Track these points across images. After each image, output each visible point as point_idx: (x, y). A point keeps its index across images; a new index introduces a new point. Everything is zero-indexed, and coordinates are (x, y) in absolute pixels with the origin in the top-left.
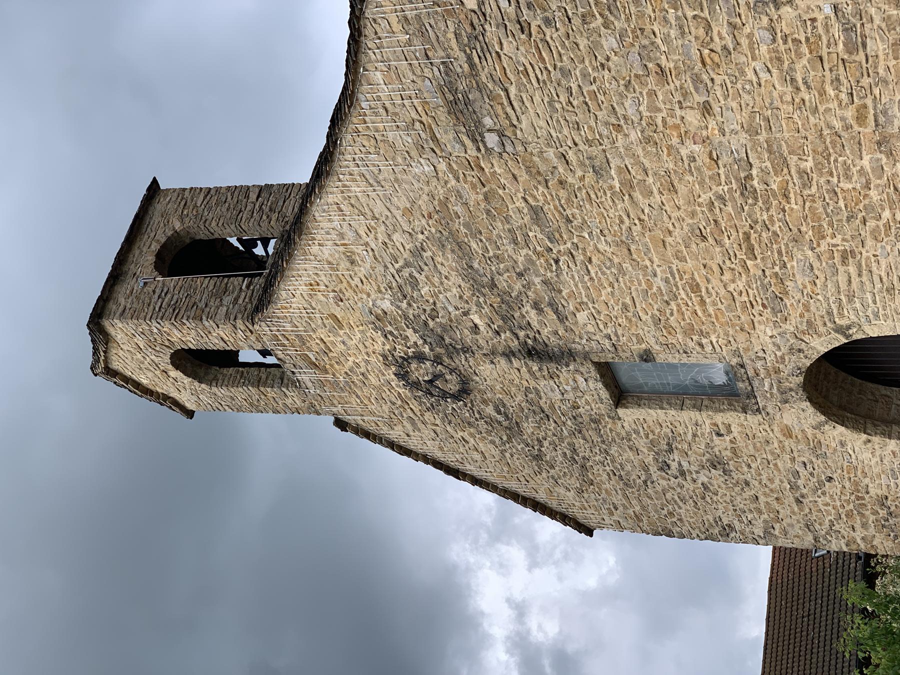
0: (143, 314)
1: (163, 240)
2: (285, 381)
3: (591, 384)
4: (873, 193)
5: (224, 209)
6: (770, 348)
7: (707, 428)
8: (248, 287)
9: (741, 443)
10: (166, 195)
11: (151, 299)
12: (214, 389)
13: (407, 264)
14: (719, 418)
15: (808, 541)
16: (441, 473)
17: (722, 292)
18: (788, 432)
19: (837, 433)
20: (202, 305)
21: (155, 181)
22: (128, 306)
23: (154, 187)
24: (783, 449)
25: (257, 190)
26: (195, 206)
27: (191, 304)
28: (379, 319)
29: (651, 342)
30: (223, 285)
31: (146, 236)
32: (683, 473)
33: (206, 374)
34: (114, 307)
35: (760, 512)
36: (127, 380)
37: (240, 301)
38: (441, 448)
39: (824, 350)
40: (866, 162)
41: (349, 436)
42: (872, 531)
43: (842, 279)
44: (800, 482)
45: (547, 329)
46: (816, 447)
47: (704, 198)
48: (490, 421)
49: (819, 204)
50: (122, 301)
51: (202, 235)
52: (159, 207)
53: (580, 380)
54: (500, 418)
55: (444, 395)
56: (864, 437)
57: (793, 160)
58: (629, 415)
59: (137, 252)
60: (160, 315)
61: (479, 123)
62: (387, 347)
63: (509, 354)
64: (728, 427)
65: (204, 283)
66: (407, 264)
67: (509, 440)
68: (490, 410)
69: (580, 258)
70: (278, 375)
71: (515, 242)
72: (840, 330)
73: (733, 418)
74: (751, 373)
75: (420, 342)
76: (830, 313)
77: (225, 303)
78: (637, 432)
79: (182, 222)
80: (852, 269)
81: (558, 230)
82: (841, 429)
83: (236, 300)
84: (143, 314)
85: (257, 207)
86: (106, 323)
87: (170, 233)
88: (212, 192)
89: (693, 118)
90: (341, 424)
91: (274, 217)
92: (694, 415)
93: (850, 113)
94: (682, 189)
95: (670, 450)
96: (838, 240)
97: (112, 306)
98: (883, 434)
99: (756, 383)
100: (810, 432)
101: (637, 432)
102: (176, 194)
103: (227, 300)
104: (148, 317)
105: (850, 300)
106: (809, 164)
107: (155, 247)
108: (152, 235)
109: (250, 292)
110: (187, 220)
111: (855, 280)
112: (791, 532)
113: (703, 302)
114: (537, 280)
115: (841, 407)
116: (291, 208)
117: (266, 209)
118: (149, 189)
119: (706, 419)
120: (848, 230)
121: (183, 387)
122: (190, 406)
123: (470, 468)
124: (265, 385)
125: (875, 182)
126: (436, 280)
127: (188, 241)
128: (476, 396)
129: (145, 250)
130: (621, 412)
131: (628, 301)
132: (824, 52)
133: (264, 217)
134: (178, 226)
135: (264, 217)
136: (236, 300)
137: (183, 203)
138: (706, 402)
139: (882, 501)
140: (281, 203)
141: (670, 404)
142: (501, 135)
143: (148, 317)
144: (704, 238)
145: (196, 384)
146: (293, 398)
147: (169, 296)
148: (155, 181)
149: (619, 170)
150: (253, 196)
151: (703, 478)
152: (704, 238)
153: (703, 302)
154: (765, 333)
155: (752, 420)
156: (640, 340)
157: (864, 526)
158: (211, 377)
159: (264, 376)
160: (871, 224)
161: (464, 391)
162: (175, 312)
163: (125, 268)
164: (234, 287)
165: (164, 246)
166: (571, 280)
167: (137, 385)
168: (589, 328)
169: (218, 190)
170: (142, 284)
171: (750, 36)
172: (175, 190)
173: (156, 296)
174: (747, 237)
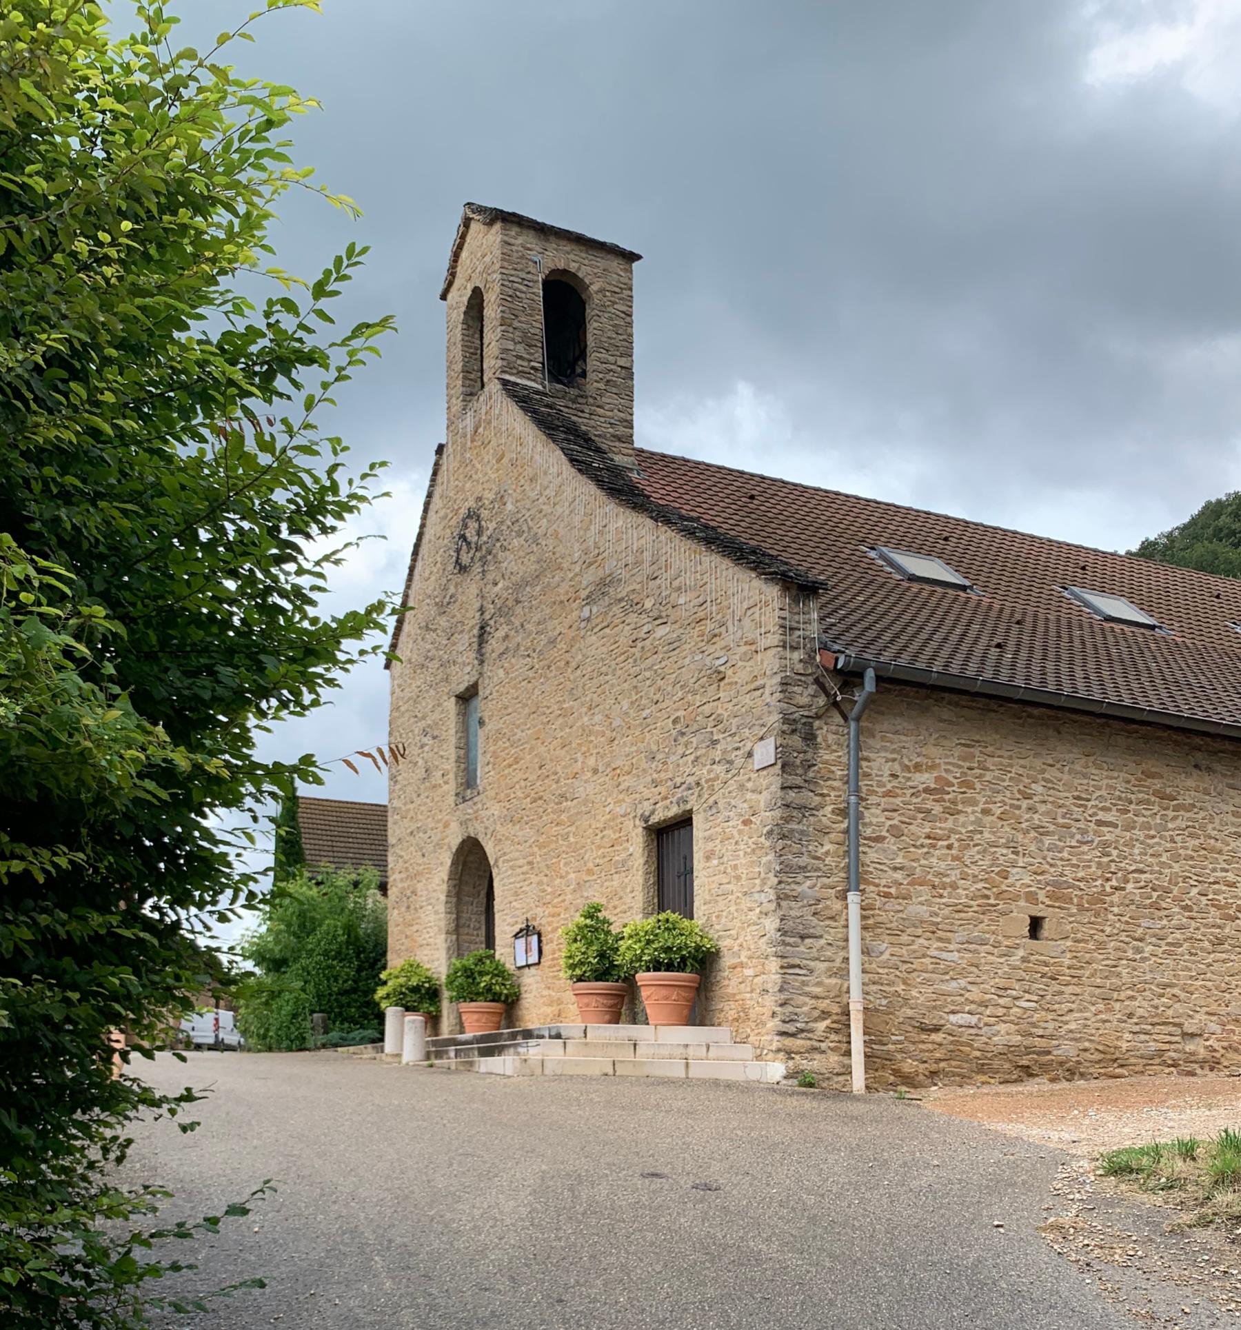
0: (506, 264)
1: (580, 275)
2: (468, 398)
3: (467, 677)
4: (558, 881)
5: (609, 334)
6: (489, 813)
7: (446, 767)
8: (533, 368)
9: (440, 791)
10: (626, 270)
11: (522, 270)
12: (460, 326)
13: (530, 528)
14: (451, 776)
15: (392, 840)
16: (414, 540)
17: (515, 780)
18: (446, 826)
19: (447, 859)
20: (516, 324)
21: (639, 257)
22: (514, 248)
23: (632, 257)
24: (439, 821)
25: (628, 365)
26: (614, 303)
27: (516, 312)
28: (501, 498)
29: (490, 726)
30: (534, 342)
31: (584, 255)
32: (422, 747)
33: (473, 318)
34: (513, 233)
35: (405, 804)
36: (463, 237)
37: (519, 362)
38: (430, 541)
39: (487, 850)
40: (572, 876)
41: (433, 458)
42: (400, 885)
43: (521, 862)
44: (421, 834)
45: (494, 645)
46: (439, 845)
47: (559, 769)
48: (446, 589)
49: (553, 846)
50: (520, 241)
51: (589, 312)
52: (615, 264)
53: (468, 669)
54: (447, 599)
55: (458, 551)
56: (446, 878)
57: (573, 829)
58: (451, 705)
59: (568, 248)
60: (506, 282)
61: (594, 602)
62: (487, 502)
63: (482, 610)
64: (446, 783)
65: (537, 323)
66: (530, 528)
67: (437, 604)
68: (452, 590)
69: (531, 674)
70: (474, 391)
71: (539, 623)
72: (496, 861)
73: (451, 787)
74: (475, 799)
75: (489, 533)
76: (505, 854)
77: (518, 347)
78: (442, 712)
79: (597, 292)
80: (525, 868)
81: (544, 659)
82: (449, 862)
83: (521, 358)
84: (506, 264)
85: (613, 367)
86: (498, 226)
87: (587, 281)
88: (628, 319)
89: (591, 761)
90: (440, 450)
91: (602, 386)
92: (453, 758)
93: (590, 865)
94: (563, 752)
95: (434, 738)
96: (539, 859)
97: (514, 230)
98: (449, 891)
99: (470, 803)
100: (446, 841)
101: (442, 712)
102: (626, 280)
103: (520, 348)
104: (504, 271)
105: (512, 868)
106: (572, 839)
107: (573, 267)
108: (586, 262)
109: (527, 370)
110: (600, 296)
111: (519, 871)
112: (396, 827)
113: (510, 766)
114: (519, 639)
115: (465, 864)
116: (609, 401)
117: (608, 377)
118: (632, 253)
119: (450, 766)
120: (542, 865)
121: (460, 296)
122: (449, 296)
123: (419, 564)
124: (465, 378)
125: (563, 881)
126: (521, 553)
127: (584, 297)
128: (458, 578)
129: (571, 256)
130: (453, 699)
131: (510, 710)
132: (616, 848)
133: (601, 376)
134: (594, 288)
135: (601, 376)
136: (521, 358)
137: (617, 290)
138: (463, 766)
139: (414, 893)
140: (614, 390)
141: (460, 738)
142: (588, 620)
143: (504, 271)
144: (540, 768)
145: (463, 309)
146: (458, 404)
147: (524, 289)
148: (639, 257)
149: (572, 707)
150: (622, 362)
151: (421, 762)
152: (540, 768)
153: (510, 766)
154: (495, 809)
155: (451, 799)
156: (491, 717)
157: (402, 880)
158: (471, 323)
159: (472, 376)
160: (545, 879)
161: (462, 569)
162: (509, 297)
163: (552, 238)
164: (532, 354)
165: (575, 276)
166: (519, 665)
167: (460, 247)
168: (495, 679)
169: (630, 324)
170: (535, 259)
171: (624, 801)
172: (630, 279)
173: (524, 276)
174: (541, 798)
